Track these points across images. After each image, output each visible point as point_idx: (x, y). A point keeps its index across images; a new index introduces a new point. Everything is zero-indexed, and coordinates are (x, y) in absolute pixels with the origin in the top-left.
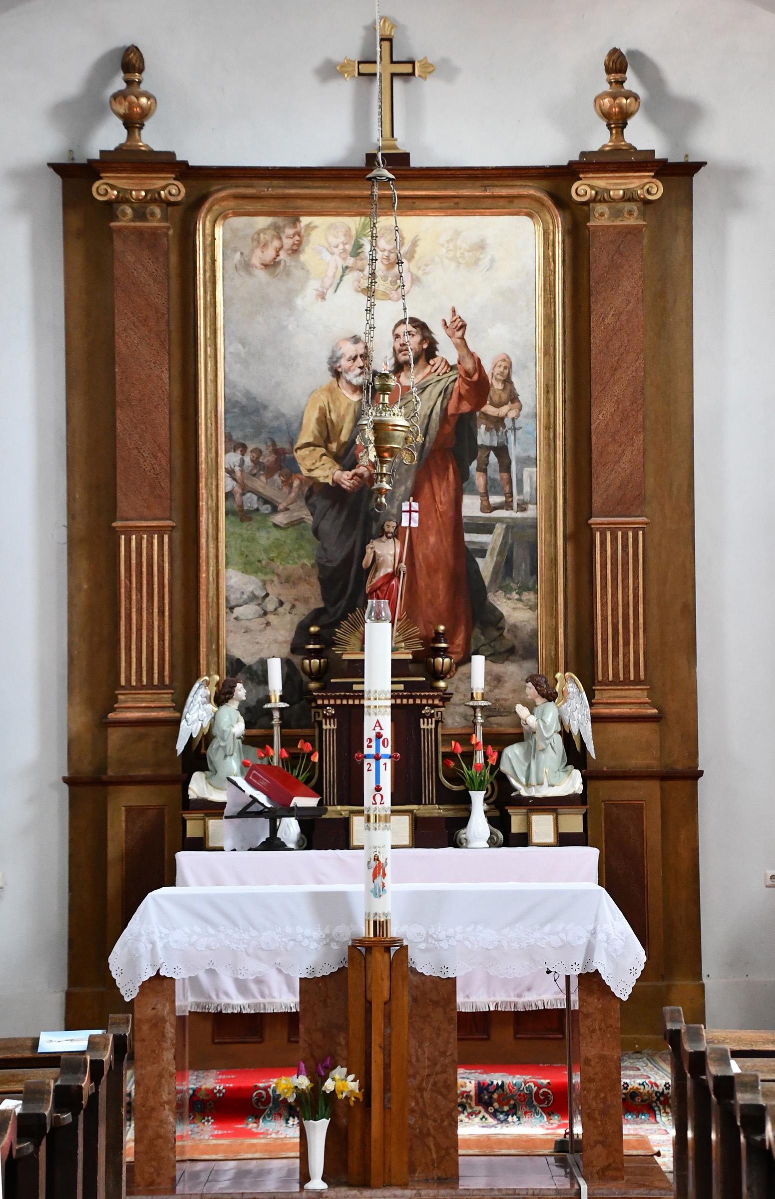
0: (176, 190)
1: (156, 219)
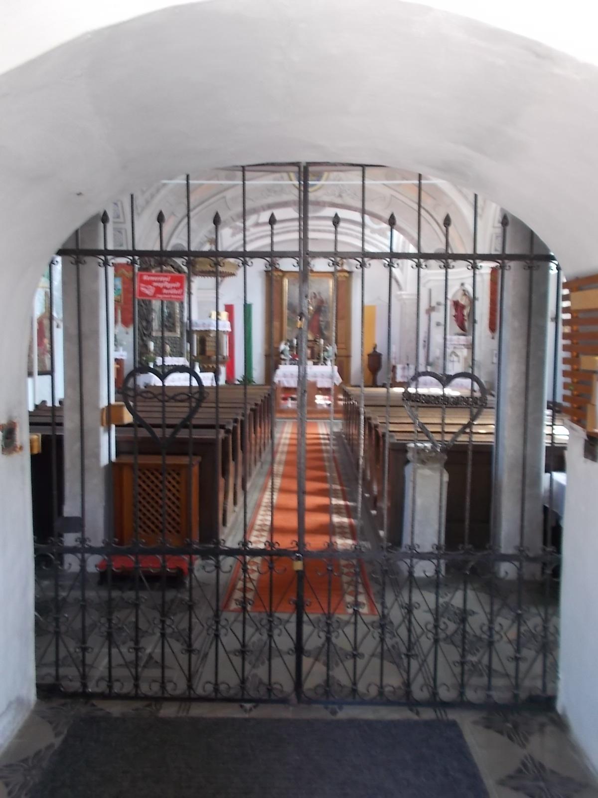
0: (280, 274)
1: (279, 278)
